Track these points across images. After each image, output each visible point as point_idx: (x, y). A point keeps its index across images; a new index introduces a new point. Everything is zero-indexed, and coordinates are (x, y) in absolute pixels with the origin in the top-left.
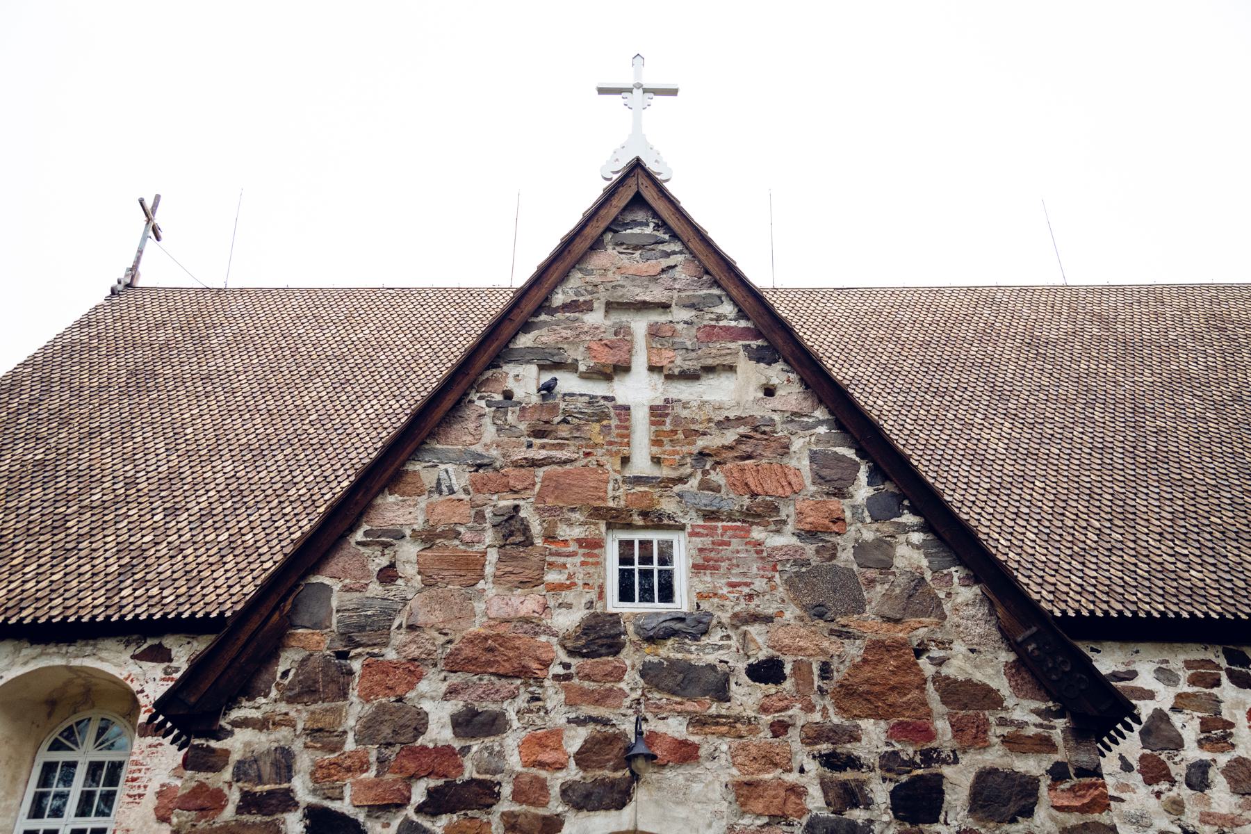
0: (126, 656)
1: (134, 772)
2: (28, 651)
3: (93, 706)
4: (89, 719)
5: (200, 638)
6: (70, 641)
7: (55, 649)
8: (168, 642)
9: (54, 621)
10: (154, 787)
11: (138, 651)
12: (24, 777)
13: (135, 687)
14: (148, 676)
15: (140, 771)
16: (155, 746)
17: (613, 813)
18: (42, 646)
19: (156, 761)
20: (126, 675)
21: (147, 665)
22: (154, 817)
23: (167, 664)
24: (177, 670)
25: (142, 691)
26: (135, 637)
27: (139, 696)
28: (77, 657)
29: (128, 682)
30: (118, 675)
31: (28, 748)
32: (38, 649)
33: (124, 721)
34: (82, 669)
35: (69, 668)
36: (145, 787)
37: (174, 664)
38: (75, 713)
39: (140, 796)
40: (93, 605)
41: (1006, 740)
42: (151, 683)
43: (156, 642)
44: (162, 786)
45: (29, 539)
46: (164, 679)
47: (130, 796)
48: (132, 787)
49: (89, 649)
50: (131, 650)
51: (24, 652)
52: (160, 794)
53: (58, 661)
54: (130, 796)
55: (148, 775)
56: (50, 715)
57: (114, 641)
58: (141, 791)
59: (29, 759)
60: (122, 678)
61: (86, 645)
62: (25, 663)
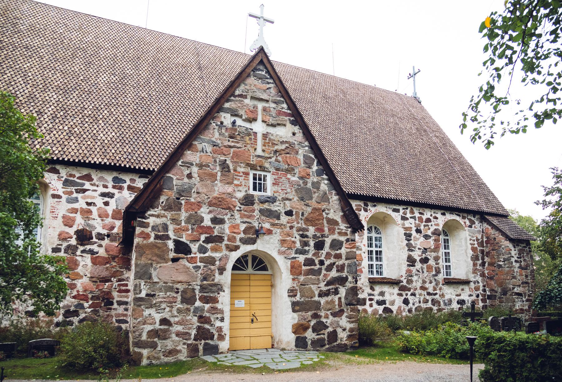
8: (58, 167)
10: (60, 215)
22: (62, 224)
24: (62, 177)
42: (53, 181)
52: (63, 217)
58: (56, 216)
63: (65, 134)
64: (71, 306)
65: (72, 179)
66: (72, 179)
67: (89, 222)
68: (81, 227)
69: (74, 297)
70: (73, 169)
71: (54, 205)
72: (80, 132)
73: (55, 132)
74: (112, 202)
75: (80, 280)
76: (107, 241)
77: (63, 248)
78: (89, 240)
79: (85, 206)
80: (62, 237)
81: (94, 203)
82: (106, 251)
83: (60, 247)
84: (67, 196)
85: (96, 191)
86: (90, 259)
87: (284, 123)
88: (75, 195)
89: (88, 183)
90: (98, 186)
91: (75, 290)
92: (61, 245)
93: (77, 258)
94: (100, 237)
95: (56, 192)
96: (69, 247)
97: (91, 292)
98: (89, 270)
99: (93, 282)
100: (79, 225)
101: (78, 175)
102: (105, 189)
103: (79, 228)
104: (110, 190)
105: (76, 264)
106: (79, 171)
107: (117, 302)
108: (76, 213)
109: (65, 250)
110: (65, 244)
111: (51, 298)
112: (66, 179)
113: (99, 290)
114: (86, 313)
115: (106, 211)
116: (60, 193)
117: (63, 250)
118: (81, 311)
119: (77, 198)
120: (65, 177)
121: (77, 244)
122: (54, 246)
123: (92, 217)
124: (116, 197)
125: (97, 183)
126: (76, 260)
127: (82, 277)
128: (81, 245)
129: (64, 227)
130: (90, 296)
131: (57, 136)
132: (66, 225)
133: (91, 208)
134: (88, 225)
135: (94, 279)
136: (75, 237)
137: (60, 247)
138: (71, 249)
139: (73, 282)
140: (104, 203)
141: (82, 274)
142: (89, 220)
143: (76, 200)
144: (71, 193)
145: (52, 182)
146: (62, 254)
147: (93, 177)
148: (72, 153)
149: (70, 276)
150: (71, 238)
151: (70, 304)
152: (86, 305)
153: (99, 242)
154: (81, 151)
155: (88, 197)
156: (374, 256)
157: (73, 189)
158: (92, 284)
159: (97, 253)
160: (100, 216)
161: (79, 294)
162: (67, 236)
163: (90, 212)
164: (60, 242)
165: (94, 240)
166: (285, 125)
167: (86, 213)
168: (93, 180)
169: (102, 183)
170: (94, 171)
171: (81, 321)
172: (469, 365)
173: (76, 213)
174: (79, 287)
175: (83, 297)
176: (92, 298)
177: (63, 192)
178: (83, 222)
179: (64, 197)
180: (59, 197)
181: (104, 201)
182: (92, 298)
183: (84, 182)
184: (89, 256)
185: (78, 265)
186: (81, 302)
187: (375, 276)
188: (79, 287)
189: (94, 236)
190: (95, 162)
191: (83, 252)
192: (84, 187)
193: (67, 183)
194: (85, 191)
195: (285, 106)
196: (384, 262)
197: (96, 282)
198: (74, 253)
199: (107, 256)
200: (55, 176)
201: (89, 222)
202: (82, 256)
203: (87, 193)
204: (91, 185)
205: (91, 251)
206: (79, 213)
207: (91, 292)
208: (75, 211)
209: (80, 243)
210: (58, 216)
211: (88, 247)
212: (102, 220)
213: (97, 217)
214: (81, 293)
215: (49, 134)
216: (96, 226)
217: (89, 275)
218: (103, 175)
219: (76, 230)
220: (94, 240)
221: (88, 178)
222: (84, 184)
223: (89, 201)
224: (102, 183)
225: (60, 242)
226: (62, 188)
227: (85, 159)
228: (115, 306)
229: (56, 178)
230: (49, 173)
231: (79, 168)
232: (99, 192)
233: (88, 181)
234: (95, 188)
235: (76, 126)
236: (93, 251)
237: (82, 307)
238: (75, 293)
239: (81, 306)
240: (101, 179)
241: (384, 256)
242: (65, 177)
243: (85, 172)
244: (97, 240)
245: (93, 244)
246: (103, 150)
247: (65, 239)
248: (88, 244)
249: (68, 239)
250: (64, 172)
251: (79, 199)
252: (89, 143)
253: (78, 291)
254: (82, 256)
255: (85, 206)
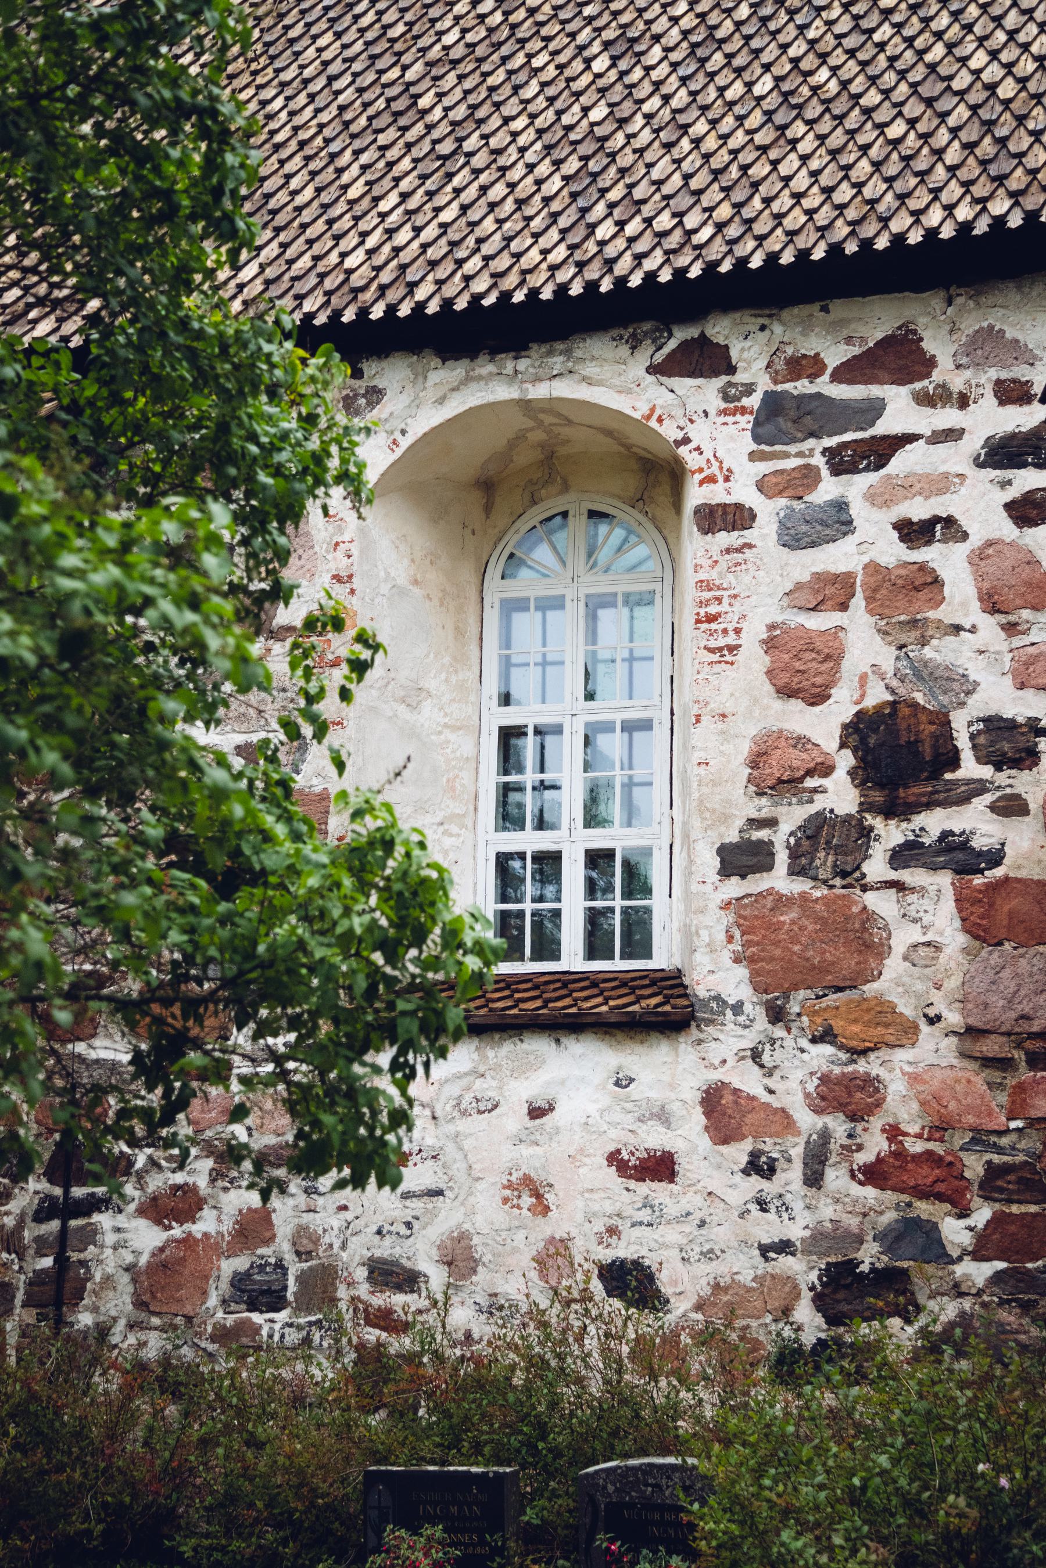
0: (637, 367)
1: (708, 603)
2: (443, 375)
3: (566, 488)
4: (565, 514)
5: (785, 314)
6: (518, 347)
7: (491, 368)
8: (719, 329)
9: (487, 302)
10: (754, 632)
11: (659, 357)
12: (474, 630)
13: (670, 432)
14: (691, 407)
15: (719, 600)
16: (739, 550)
17: (958, 923)
18: (466, 362)
19: (747, 579)
20: (645, 410)
21: (684, 384)
22: (769, 688)
23: (724, 379)
24: (749, 389)
25: (686, 441)
26: (647, 326)
27: (683, 451)
28: (537, 379)
29: (653, 423)
30: (629, 412)
31: (468, 575)
32: (457, 371)
33: (634, 512)
34: (552, 406)
35: (525, 405)
36: (738, 631)
37: (740, 377)
38: (534, 503)
39: (732, 649)
40: (544, 266)
41: (825, 1136)
42: (700, 421)
43: (692, 332)
44: (772, 627)
45: (357, 144)
46: (724, 412)
47: (712, 651)
48: (712, 633)
49: (558, 362)
50: (644, 357)
51: (434, 377)
52: (770, 644)
53: (503, 392)
54: (712, 651)
55: (737, 607)
56: (488, 509)
57: (607, 338)
58: (731, 639)
59: (473, 594)
60: (637, 415)
61: (550, 353)
62: (441, 401)
63: (756, 119)
64: (860, 1241)
65: (802, 387)
66: (802, 387)
67: (928, 652)
68: (877, 696)
69: (873, 1174)
70: (807, 326)
71: (714, 574)
72: (844, 84)
73: (701, 127)
75: (901, 1056)
77: (780, 838)
78: (936, 775)
79: (892, 552)
80: (773, 771)
81: (949, 522)
83: (763, 834)
84: (783, 502)
85: (952, 435)
86: (948, 905)
88: (829, 488)
89: (904, 391)
90: (963, 402)
91: (877, 1123)
92: (771, 823)
93: (872, 900)
95: (717, 494)
96: (816, 831)
97: (980, 1139)
98: (953, 983)
99: (987, 1062)
100: (863, 679)
101: (835, 355)
102: (1012, 410)
103: (870, 702)
105: (867, 942)
106: (843, 323)
108: (844, 607)
109: (795, 854)
110: (792, 817)
112: (770, 398)
113: (1033, 1123)
114: (958, 1291)
115: (1033, 562)
116: (743, 492)
117: (782, 858)
118: (924, 1279)
119: (841, 505)
120: (764, 384)
121: (865, 807)
122: (732, 836)
123: (944, 614)
125: (957, 383)
126: (868, 916)
127: (908, 1033)
128: (892, 810)
129: (778, 705)
130: (974, 1166)
131: (711, 143)
132: (787, 692)
133: (931, 554)
134: (924, 674)
135: (991, 1047)
136: (846, 760)
137: (763, 834)
138: (836, 847)
139: (861, 1066)
140: (1009, 507)
141: (906, 1009)
142: (924, 642)
143: (838, 521)
144: (808, 477)
145: (692, 432)
146: (779, 879)
147: (929, 346)
148: (796, 219)
149: (838, 1025)
150: (826, 769)
151: (853, 1222)
152: (956, 1232)
153: (1002, 778)
154: (844, 193)
155: (907, 487)
157: (814, 451)
158: (979, 1081)
159: (995, 858)
160: (992, 605)
161: (900, 1154)
162: (800, 759)
163: (927, 583)
164: (764, 807)
165: (970, 768)
167: (906, 597)
168: (931, 363)
169: (993, 374)
170: (935, 300)
171: (932, 1345)
173: (844, 607)
174: (901, 1104)
175: (927, 1175)
176: (992, 1183)
177: (761, 486)
178: (886, 657)
179: (768, 512)
180: (737, 517)
181: (1013, 493)
182: (992, 1183)
183: (875, 391)
184: (945, 879)
185: (880, 950)
186: (924, 1209)
188: (901, 1104)
189: (963, 742)
190: (932, 233)
191: (901, 856)
192: (883, 427)
193: (779, 420)
194: (882, 451)
197: (1004, 1064)
198: (849, 874)
200: (704, 393)
201: (928, 652)
202: (898, 886)
203: (900, 463)
204: (925, 400)
205: (951, 848)
206: (858, 602)
207: (980, 1139)
208: (832, 592)
209: (878, 797)
210: (745, 639)
211: (934, 823)
212: (1011, 629)
213: (974, 614)
214: (916, 1147)
215: (668, 146)
216: (975, 669)
217: (953, 1018)
218: (995, 319)
219: (848, 714)
220: (970, 768)
221: (899, 358)
222: (875, 409)
223: (918, 510)
224: (993, 374)
225: (764, 807)
226: (753, 456)
227: (868, 230)
229: (716, 403)
230: (676, 382)
231: (839, 308)
232: (973, 444)
233: (902, 378)
234: (948, 417)
235: (823, 57)
236: (964, 846)
237: (934, 1249)
238: (875, 1145)
239: (917, 1238)
240: (985, 345)
242: (764, 384)
243: (877, 321)
244: (986, 772)
245: (965, 800)
246: (987, 149)
247: (789, 785)
248: (929, 805)
249: (810, 783)
250: (753, 353)
251: (858, 510)
252: (896, 130)
253: (894, 1132)
254: (898, 886)
255: (892, 552)
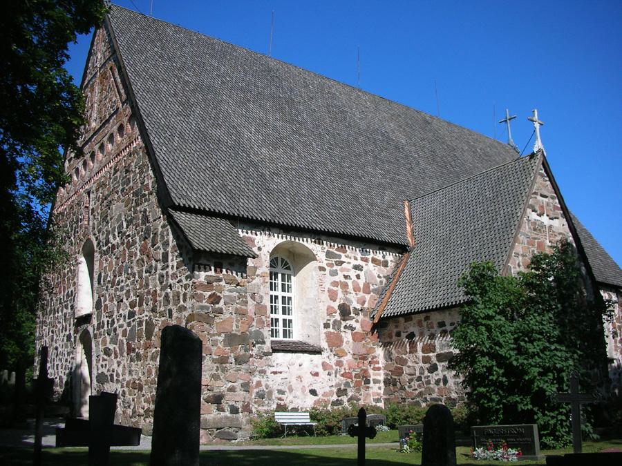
10: (326, 290)
22: (329, 298)
68: (342, 302)
74: (362, 274)
75: (345, 358)
76: (361, 317)
77: (331, 322)
79: (343, 279)
82: (362, 327)
87: (557, 216)
94: (357, 312)
104: (359, 262)
107: (373, 380)
111: (494, 375)
119: (336, 270)
124: (364, 269)
130: (354, 374)
135: (355, 357)
136: (339, 311)
156: (280, 305)
164: (328, 317)
166: (558, 218)
172: (368, 456)
187: (281, 338)
195: (557, 201)
196: (294, 316)
199: (362, 332)
203: (344, 265)
213: (352, 292)
214: (347, 371)
220: (352, 315)
228: (372, 384)
241: (294, 305)
255: (343, 279)
